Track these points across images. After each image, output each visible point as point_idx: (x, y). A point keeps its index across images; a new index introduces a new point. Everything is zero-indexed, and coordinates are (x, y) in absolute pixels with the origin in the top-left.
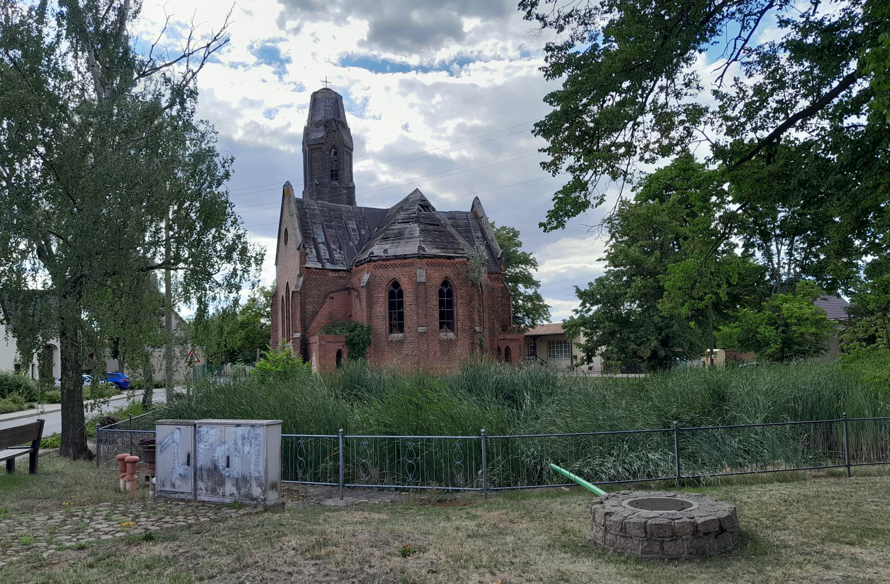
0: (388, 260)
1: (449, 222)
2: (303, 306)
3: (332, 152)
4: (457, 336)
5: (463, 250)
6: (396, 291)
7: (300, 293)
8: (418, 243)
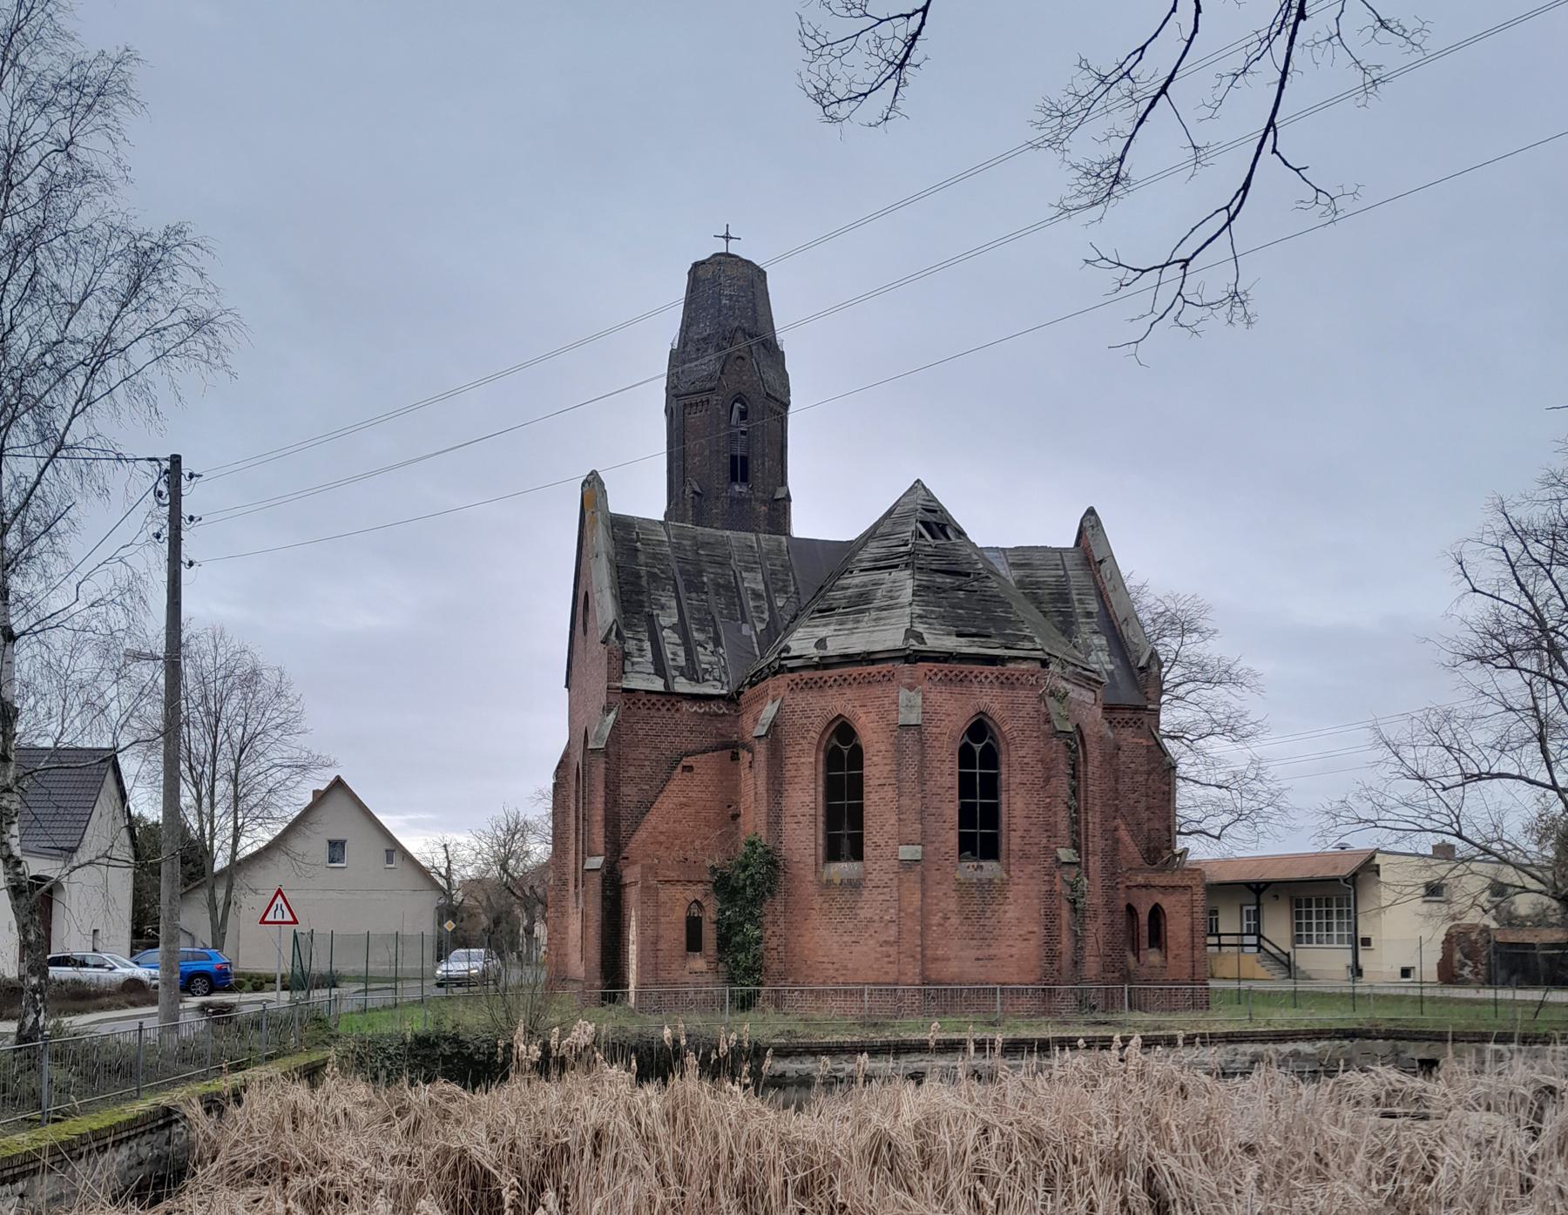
0: (827, 667)
1: (1011, 576)
2: (612, 787)
3: (736, 413)
4: (1008, 872)
5: (1031, 639)
6: (846, 749)
7: (606, 753)
8: (907, 620)
